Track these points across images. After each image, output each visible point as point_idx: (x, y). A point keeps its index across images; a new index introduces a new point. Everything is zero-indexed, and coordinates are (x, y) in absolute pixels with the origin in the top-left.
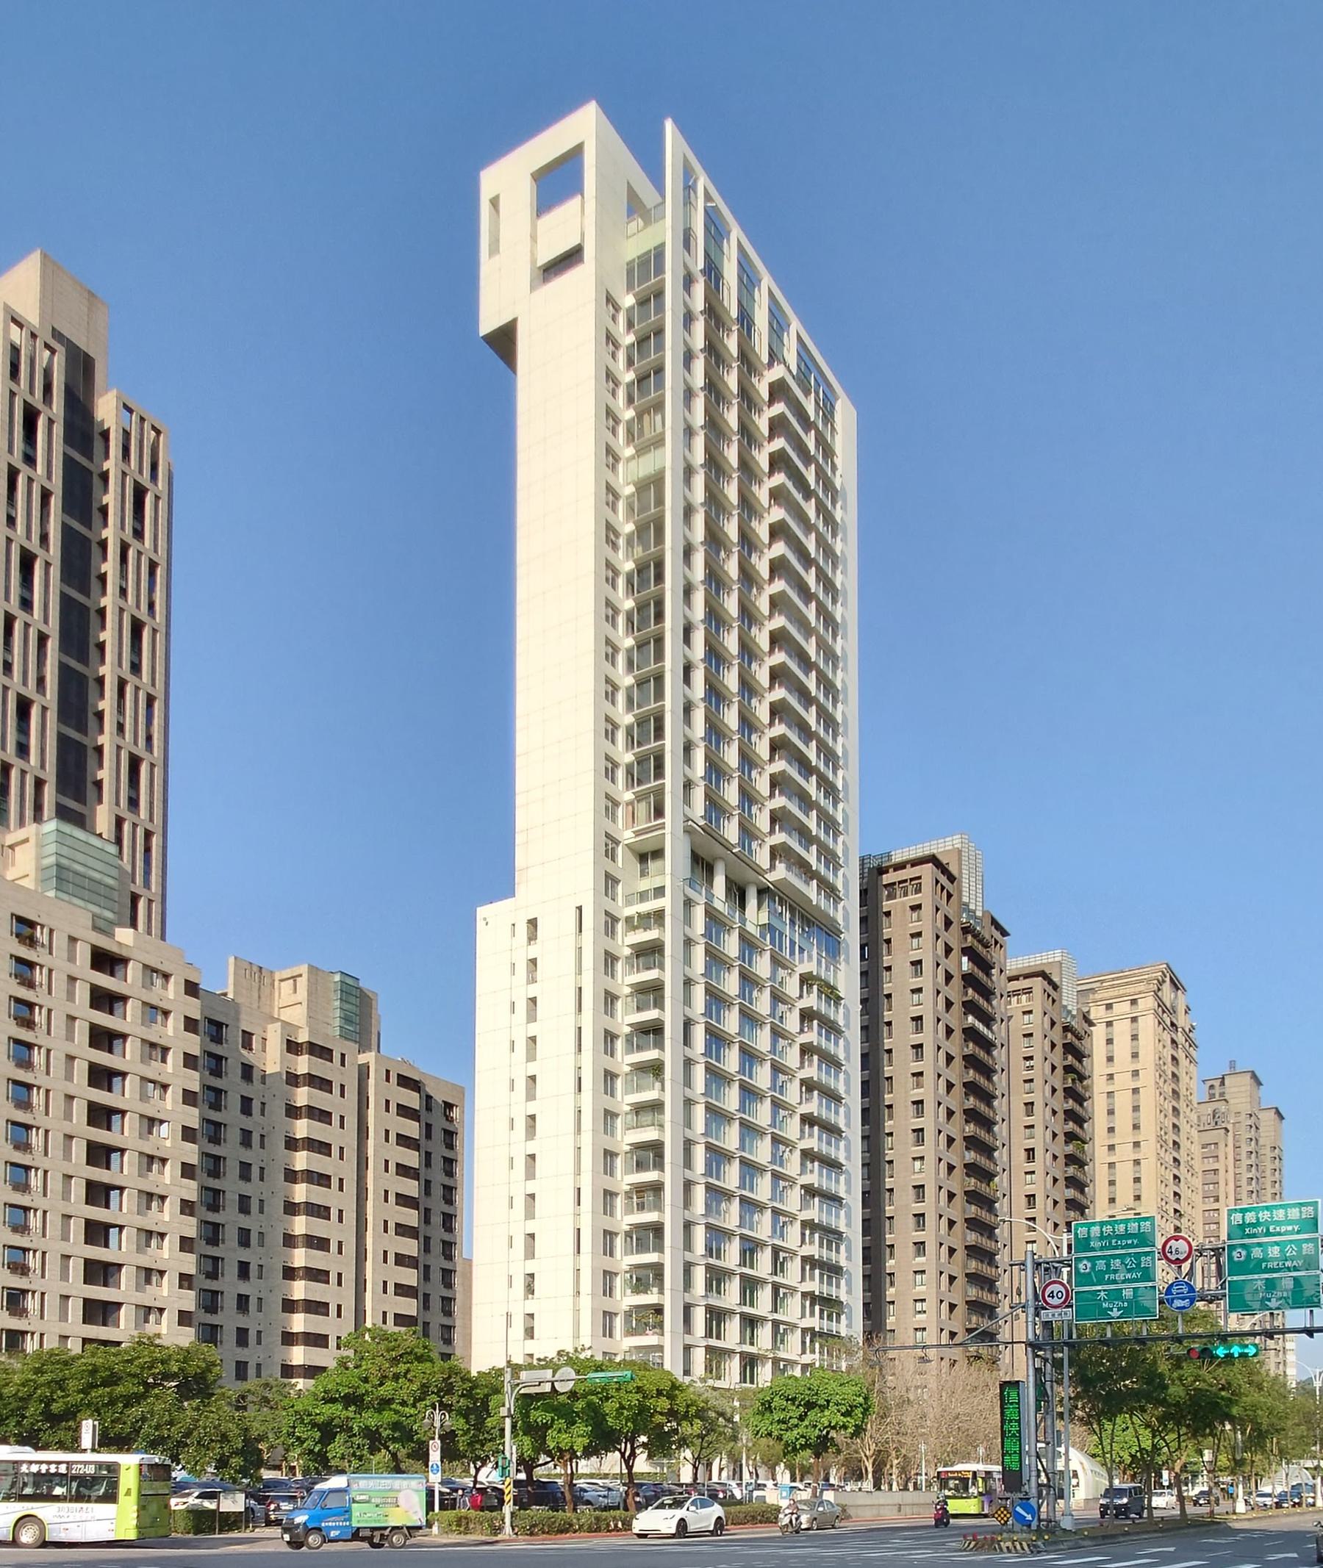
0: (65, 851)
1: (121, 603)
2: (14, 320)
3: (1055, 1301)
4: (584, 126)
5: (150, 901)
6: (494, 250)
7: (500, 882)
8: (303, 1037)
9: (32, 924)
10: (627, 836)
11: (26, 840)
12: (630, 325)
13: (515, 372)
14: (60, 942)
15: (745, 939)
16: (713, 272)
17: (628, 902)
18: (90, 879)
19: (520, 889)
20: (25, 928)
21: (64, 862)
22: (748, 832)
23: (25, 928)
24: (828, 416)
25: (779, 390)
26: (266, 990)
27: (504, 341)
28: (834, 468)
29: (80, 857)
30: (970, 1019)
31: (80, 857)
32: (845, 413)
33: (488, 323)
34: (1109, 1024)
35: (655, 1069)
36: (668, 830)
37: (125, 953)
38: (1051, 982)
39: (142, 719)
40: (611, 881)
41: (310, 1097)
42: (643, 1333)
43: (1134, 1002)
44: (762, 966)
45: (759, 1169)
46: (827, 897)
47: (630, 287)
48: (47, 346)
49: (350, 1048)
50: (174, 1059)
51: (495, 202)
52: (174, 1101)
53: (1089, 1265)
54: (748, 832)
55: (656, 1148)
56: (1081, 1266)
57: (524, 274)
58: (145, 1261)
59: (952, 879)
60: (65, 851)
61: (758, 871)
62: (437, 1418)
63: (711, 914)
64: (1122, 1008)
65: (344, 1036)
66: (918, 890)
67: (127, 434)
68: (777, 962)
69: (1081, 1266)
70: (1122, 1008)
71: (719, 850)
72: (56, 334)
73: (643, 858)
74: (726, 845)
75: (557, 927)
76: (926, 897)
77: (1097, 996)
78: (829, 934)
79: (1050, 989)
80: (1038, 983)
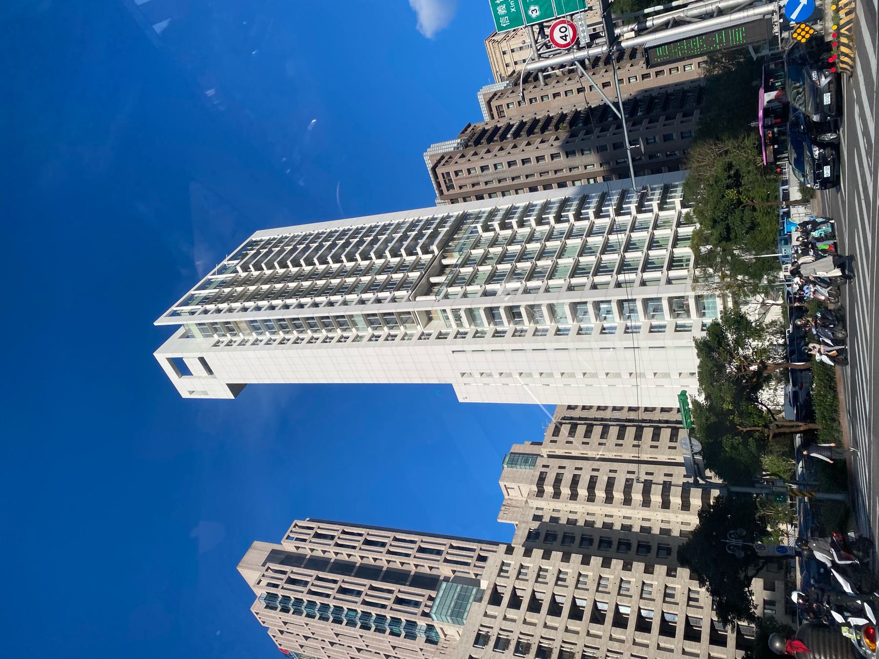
0: (444, 611)
1: (358, 549)
2: (258, 583)
3: (570, 32)
4: (162, 356)
5: (481, 549)
6: (206, 393)
7: (447, 389)
8: (535, 488)
9: (479, 635)
10: (420, 329)
11: (442, 629)
12: (224, 335)
13: (246, 384)
14: (487, 621)
15: (464, 264)
16: (206, 300)
17: (450, 326)
18: (454, 607)
19: (449, 382)
20: (481, 639)
21: (449, 613)
22: (415, 267)
23: (481, 639)
24: (256, 243)
25: (245, 268)
26: (514, 503)
27: (234, 388)
28: (274, 239)
29: (448, 603)
30: (509, 136)
31: (448, 603)
32: (255, 237)
33: (230, 396)
34: (516, 63)
35: (531, 308)
36: (416, 310)
37: (492, 586)
38: (493, 97)
39: (403, 544)
40: (441, 336)
41: (566, 486)
42: (688, 306)
43: (504, 53)
44: (478, 252)
45: (585, 244)
46: (446, 222)
47: (212, 336)
48: (267, 570)
49: (540, 462)
50: (545, 564)
51: (191, 392)
52: (568, 567)
53: (532, 8)
54: (415, 267)
55: (574, 306)
56: (534, 15)
57: (210, 380)
58: (659, 597)
59: (443, 158)
60: (444, 611)
61: (434, 258)
62: (734, 542)
63: (451, 284)
64: (508, 58)
65: (534, 464)
66: (448, 174)
67: (297, 539)
68: (476, 246)
69: (534, 15)
70: (508, 58)
71: (424, 280)
72: (264, 565)
73: (430, 319)
74: (421, 277)
75: (463, 362)
76: (451, 169)
77: (503, 72)
78: (463, 218)
79: (496, 97)
80: (494, 104)
